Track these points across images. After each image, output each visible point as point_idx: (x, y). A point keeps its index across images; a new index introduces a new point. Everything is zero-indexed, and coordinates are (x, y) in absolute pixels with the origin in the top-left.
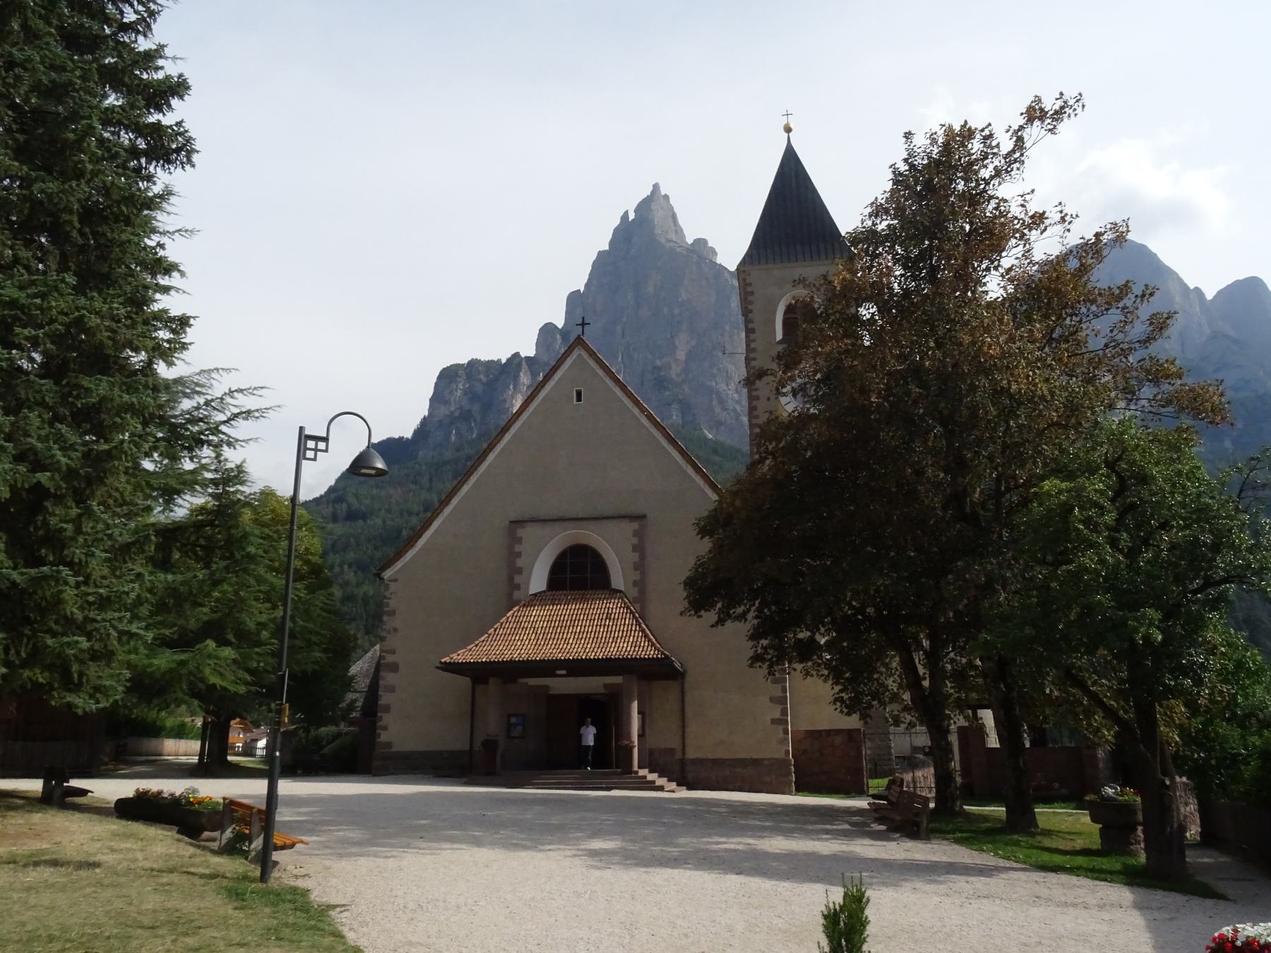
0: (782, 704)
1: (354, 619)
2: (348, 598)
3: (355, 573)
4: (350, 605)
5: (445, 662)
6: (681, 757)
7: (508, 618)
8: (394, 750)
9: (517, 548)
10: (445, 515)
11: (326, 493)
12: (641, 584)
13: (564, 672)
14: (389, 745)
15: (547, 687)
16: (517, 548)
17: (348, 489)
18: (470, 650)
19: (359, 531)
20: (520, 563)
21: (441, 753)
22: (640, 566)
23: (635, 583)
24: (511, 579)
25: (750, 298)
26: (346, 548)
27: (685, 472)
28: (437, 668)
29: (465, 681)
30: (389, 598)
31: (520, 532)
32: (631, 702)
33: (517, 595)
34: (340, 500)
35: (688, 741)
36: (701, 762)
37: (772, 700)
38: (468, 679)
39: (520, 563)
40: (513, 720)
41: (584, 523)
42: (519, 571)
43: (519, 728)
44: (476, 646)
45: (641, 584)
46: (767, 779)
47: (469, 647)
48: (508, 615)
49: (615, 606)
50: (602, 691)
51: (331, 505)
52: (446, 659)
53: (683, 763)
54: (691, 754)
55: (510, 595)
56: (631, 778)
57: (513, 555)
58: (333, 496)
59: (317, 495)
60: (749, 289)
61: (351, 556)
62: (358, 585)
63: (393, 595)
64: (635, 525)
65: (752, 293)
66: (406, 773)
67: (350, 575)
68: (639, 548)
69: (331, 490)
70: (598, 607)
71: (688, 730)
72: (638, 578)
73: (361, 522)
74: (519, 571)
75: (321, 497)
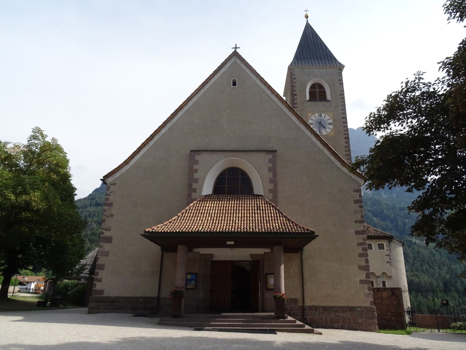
0: (366, 270)
1: (95, 242)
2: (93, 234)
3: (97, 225)
4: (94, 236)
5: (149, 231)
6: (302, 305)
7: (191, 207)
8: (105, 295)
9: (195, 167)
10: (150, 146)
11: (88, 196)
12: (274, 192)
13: (232, 243)
14: (102, 292)
15: (212, 255)
16: (195, 167)
17: (96, 195)
18: (166, 225)
19: (100, 210)
20: (196, 176)
21: (137, 298)
22: (273, 181)
23: (270, 191)
24: (190, 185)
25: (294, 81)
26: (94, 216)
27: (299, 128)
28: (142, 235)
29: (155, 249)
30: (109, 195)
31: (198, 158)
32: (281, 265)
33: (194, 195)
34: (93, 199)
35: (306, 295)
36: (316, 308)
37: (360, 268)
38: (158, 248)
39: (196, 176)
40: (189, 277)
41: (238, 154)
42: (196, 181)
43: (193, 282)
44: (170, 223)
45: (274, 192)
46: (360, 321)
47: (165, 223)
48: (191, 205)
49: (259, 202)
50: (250, 259)
51: (90, 200)
52: (150, 230)
53: (303, 308)
54: (308, 303)
55: (190, 195)
56: (286, 322)
57: (192, 171)
58: (90, 197)
59: (85, 197)
60: (293, 77)
61: (95, 219)
62: (97, 229)
63: (112, 193)
64: (270, 156)
65: (295, 78)
66: (112, 312)
67: (94, 226)
68: (273, 170)
69: (90, 195)
70: (249, 203)
71: (306, 286)
72: (272, 187)
73: (100, 207)
74: (196, 181)
75: (86, 197)
